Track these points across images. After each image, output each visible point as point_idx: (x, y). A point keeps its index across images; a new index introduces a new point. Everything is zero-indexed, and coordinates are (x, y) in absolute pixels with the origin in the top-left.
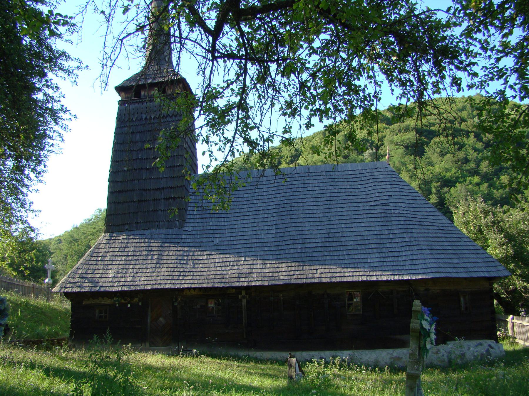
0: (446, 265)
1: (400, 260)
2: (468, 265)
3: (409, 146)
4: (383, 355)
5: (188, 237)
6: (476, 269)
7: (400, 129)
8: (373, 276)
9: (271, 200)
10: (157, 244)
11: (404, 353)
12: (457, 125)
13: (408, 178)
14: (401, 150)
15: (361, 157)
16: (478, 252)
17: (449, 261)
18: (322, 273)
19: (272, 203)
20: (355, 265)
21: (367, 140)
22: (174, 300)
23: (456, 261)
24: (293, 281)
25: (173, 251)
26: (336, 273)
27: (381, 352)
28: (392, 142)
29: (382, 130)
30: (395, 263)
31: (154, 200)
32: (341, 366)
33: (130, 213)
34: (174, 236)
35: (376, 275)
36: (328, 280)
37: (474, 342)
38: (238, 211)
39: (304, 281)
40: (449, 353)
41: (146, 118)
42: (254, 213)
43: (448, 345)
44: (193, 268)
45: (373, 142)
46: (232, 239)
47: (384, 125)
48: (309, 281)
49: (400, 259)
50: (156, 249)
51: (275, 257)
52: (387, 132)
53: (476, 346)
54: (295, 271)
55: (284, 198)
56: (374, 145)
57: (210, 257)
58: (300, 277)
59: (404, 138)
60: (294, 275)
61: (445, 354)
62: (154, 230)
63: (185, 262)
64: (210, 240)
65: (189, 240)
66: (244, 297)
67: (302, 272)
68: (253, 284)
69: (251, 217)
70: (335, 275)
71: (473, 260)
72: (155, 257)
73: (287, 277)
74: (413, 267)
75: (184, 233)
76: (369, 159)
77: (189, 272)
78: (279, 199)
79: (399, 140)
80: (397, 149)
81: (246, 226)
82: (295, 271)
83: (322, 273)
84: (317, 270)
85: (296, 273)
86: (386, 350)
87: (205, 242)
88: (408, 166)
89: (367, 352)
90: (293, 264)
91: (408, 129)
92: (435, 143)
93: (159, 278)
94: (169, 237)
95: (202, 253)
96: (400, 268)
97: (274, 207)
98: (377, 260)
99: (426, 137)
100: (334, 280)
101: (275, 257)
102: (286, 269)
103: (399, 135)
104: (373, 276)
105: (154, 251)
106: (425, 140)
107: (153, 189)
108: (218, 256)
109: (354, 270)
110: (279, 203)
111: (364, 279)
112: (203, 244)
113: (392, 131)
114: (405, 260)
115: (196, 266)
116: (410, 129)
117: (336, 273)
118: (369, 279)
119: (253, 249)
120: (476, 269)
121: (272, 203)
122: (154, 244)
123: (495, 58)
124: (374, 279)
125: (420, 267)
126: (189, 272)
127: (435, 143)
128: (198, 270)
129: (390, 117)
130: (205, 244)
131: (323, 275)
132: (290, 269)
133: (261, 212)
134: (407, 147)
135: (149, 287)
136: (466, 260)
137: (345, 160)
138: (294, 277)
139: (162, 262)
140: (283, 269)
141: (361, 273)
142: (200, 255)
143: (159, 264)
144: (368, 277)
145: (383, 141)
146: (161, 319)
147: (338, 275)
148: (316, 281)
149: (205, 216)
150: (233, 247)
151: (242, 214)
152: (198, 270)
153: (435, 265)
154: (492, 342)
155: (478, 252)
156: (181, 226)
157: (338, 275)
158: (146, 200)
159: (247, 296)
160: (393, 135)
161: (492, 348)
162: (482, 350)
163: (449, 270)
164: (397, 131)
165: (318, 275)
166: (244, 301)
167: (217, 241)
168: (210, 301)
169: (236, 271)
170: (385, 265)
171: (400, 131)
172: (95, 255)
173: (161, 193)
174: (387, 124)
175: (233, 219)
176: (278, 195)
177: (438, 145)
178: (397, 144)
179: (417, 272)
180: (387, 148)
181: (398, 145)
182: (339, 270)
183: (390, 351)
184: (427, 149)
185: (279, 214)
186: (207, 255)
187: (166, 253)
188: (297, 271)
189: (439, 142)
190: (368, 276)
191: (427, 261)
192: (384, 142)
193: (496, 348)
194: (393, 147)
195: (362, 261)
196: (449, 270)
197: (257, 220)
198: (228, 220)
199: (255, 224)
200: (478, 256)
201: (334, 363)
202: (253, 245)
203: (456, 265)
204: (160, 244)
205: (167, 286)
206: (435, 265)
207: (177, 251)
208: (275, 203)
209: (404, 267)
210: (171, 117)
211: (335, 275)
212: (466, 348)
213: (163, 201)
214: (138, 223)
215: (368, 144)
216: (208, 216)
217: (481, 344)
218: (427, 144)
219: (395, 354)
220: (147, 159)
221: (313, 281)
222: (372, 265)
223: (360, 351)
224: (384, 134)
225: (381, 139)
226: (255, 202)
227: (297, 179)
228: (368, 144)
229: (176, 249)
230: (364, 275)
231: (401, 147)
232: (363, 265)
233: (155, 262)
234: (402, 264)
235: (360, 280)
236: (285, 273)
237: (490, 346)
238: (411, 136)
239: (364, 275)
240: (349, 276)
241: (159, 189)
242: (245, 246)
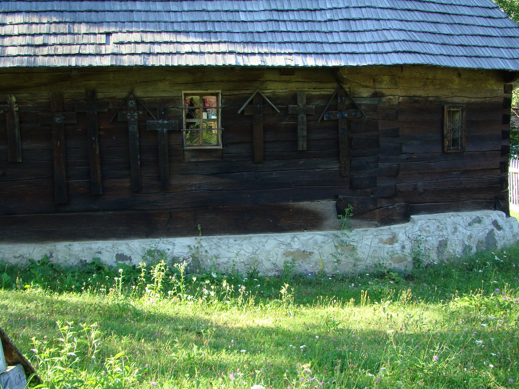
0: (426, 38)
1: (319, 19)
2: (473, 41)
4: (268, 247)
6: (487, 52)
8: (253, 54)
11: (316, 243)
16: (491, 13)
17: (432, 28)
18: (122, 43)
20: (209, 34)
23: (446, 29)
24: (41, 62)
26: (160, 43)
27: (264, 240)
30: (307, 27)
32: (167, 286)
35: (259, 53)
36: (137, 61)
37: (467, 216)
39: (73, 62)
40: (416, 241)
48: (85, 62)
49: (318, 16)
53: (470, 224)
54: (48, 34)
60: (45, 45)
67: (68, 39)
70: (157, 49)
71: (481, 31)
73: (25, 51)
74: (351, 38)
82: (48, 34)
83: (122, 43)
84: (108, 34)
85: (52, 40)
86: (275, 235)
89: (231, 241)
96: (318, 39)
98: (263, 16)
100: (152, 61)
102: (23, 29)
104: (253, 54)
109: (205, 40)
111: (231, 60)
114: (331, 20)
117: (160, 43)
118: (242, 61)
120: (487, 52)
123: (42, 383)
124: (255, 61)
125: (367, 37)
131: (124, 49)
132: (35, 29)
136: (467, 30)
138: (45, 51)
140: (16, 30)
141: (223, 48)
144: (240, 58)
147: (165, 48)
148: (106, 62)
153: (403, 36)
154: (496, 215)
155: (491, 13)
157: (165, 48)
161: (499, 228)
162: (479, 232)
163: (434, 49)
165: (111, 48)
170: (283, 28)
179: (361, 49)
182: (166, 37)
183: (286, 237)
188: (55, 34)
190: (239, 54)
191: (383, 25)
193: (506, 228)
195: (225, 17)
196: (434, 49)
200: (492, 22)
201: (149, 279)
203: (447, 40)
206: (403, 36)
209: (329, 36)
211: (157, 49)
212: (450, 229)
217: (479, 221)
219: (296, 245)
221: (97, 62)
222: (251, 28)
223: (215, 239)
230: (231, 53)
232: (228, 27)
234: (324, 29)
235: (220, 63)
236: (21, 40)
237: (495, 223)
239: (231, 53)
240: (192, 53)
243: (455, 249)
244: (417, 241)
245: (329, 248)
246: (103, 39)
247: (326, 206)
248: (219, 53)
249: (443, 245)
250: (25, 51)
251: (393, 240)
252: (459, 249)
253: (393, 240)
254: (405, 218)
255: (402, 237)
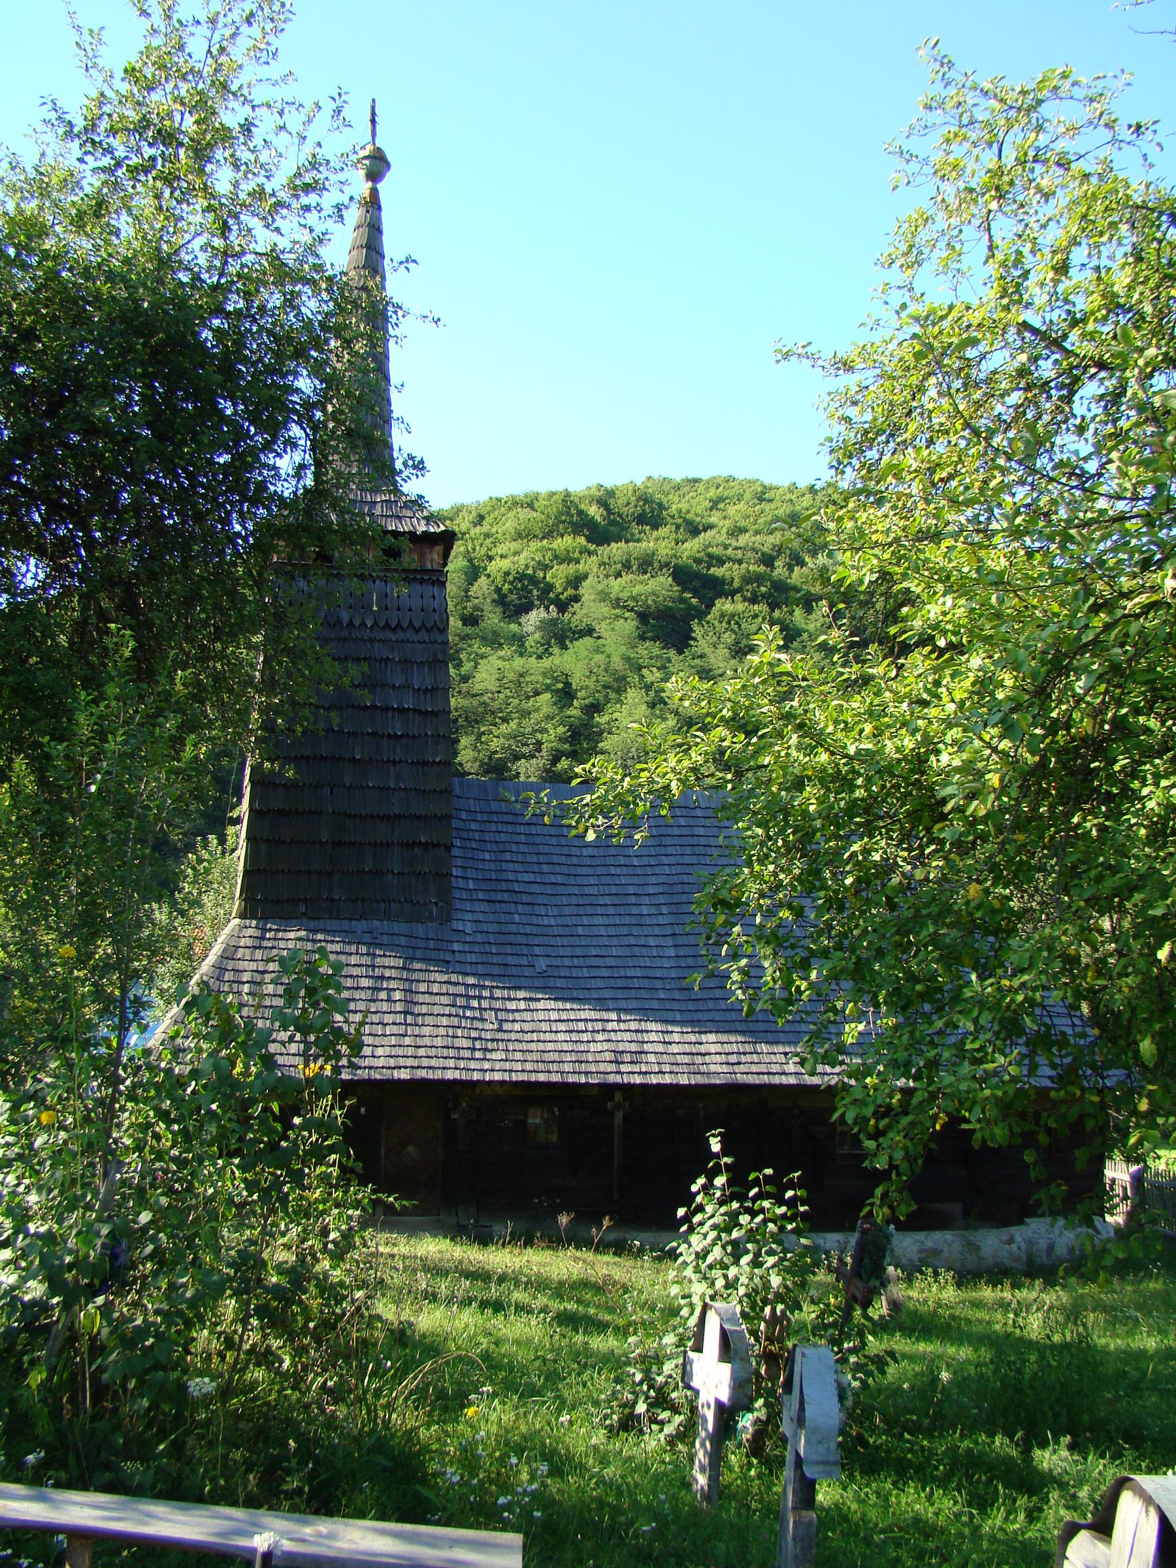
3: (650, 615)
5: (467, 948)
7: (628, 561)
9: (649, 871)
10: (393, 962)
12: (780, 570)
13: (644, 707)
14: (630, 625)
15: (513, 627)
19: (653, 880)
21: (533, 580)
22: (451, 1105)
24: (741, 1079)
25: (436, 983)
28: (603, 596)
29: (576, 555)
31: (375, 844)
33: (310, 872)
34: (432, 944)
38: (576, 890)
41: (351, 624)
42: (617, 900)
43: (1027, 1225)
44: (500, 1030)
45: (550, 587)
46: (576, 962)
47: (582, 540)
50: (394, 973)
51: (688, 1017)
52: (589, 564)
55: (679, 869)
56: (552, 595)
57: (533, 1005)
58: (754, 1068)
59: (638, 589)
60: (739, 1063)
61: (1023, 1246)
62: (376, 923)
63: (477, 1014)
64: (524, 961)
65: (473, 958)
66: (618, 1106)
68: (654, 1080)
69: (611, 910)
72: (397, 995)
75: (455, 937)
76: (537, 636)
77: (493, 1040)
78: (667, 870)
79: (625, 595)
80: (617, 617)
81: (603, 931)
87: (515, 962)
88: (645, 671)
90: (732, 1038)
91: (651, 564)
92: (722, 615)
93: (421, 1052)
94: (421, 944)
95: (512, 994)
97: (661, 889)
99: (696, 593)
101: (688, 1017)
103: (626, 578)
105: (390, 978)
106: (694, 601)
107: (372, 816)
108: (552, 1004)
110: (670, 880)
112: (510, 971)
113: (604, 564)
115: (506, 1026)
116: (656, 565)
119: (633, 993)
121: (653, 880)
122: (386, 962)
126: (493, 1040)
127: (722, 615)
128: (513, 1036)
129: (598, 518)
130: (514, 971)
133: (633, 900)
134: (643, 617)
135: (404, 1075)
137: (469, 630)
139: (416, 1010)
142: (509, 999)
143: (412, 1014)
145: (576, 588)
146: (410, 1149)
149: (499, 897)
150: (583, 983)
151: (587, 900)
152: (513, 1036)
156: (446, 917)
158: (354, 844)
159: (627, 1104)
160: (607, 576)
164: (619, 566)
166: (619, 1116)
167: (542, 964)
168: (532, 1111)
169: (606, 1046)
171: (627, 566)
172: (228, 976)
173: (393, 829)
174: (589, 540)
175: (566, 911)
176: (665, 860)
177: (729, 623)
178: (617, 603)
180: (589, 609)
181: (618, 606)
183: (920, 1236)
184: (698, 631)
185: (675, 909)
186: (525, 999)
187: (423, 987)
189: (733, 615)
192: (581, 591)
194: (605, 610)
197: (627, 920)
198: (555, 911)
199: (625, 931)
202: (630, 983)
204: (401, 963)
205: (450, 1075)
207: (450, 983)
208: (661, 879)
210: (417, 631)
213: (396, 848)
214: (333, 900)
215: (535, 592)
216: (505, 896)
218: (701, 615)
219: (929, 1244)
220: (355, 733)
224: (581, 567)
225: (576, 581)
226: (613, 870)
227: (702, 822)
228: (535, 592)
229: (445, 978)
231: (627, 614)
233: (399, 1007)
236: (718, 1058)
238: (660, 586)
241: (387, 818)
242: (612, 983)
243: (1060, 1250)
244: (1030, 1243)
245: (957, 1247)
246: (782, 1059)
247: (954, 1208)
248: (381, 818)
249: (1051, 1247)
250: (725, 1069)
251: (1011, 1241)
252: (1065, 1251)
253: (1011, 1241)
254: (1020, 1222)
255: (1018, 1238)
